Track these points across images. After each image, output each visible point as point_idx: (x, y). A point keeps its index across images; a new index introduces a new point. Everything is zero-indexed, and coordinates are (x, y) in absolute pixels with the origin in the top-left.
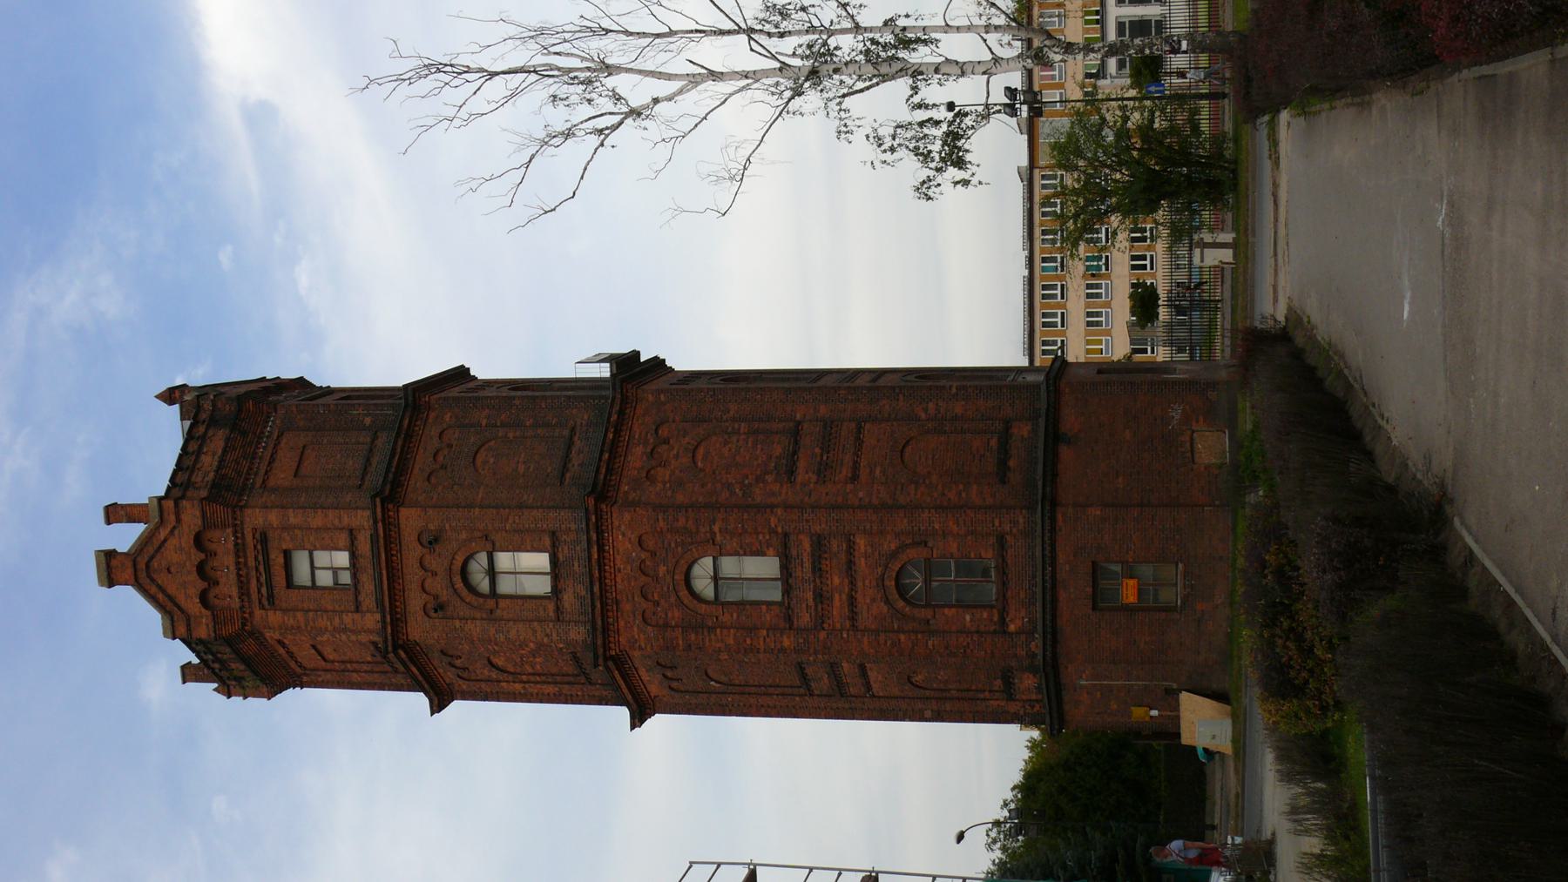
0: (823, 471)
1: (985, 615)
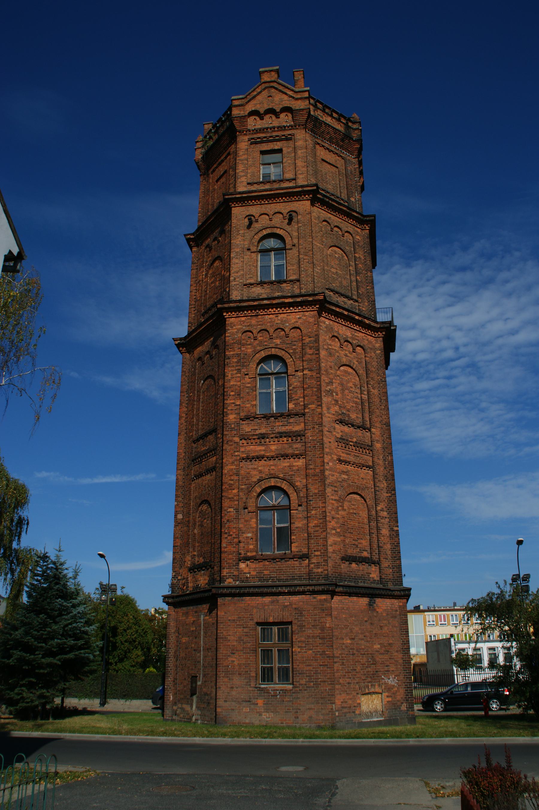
0: (343, 441)
1: (251, 547)
